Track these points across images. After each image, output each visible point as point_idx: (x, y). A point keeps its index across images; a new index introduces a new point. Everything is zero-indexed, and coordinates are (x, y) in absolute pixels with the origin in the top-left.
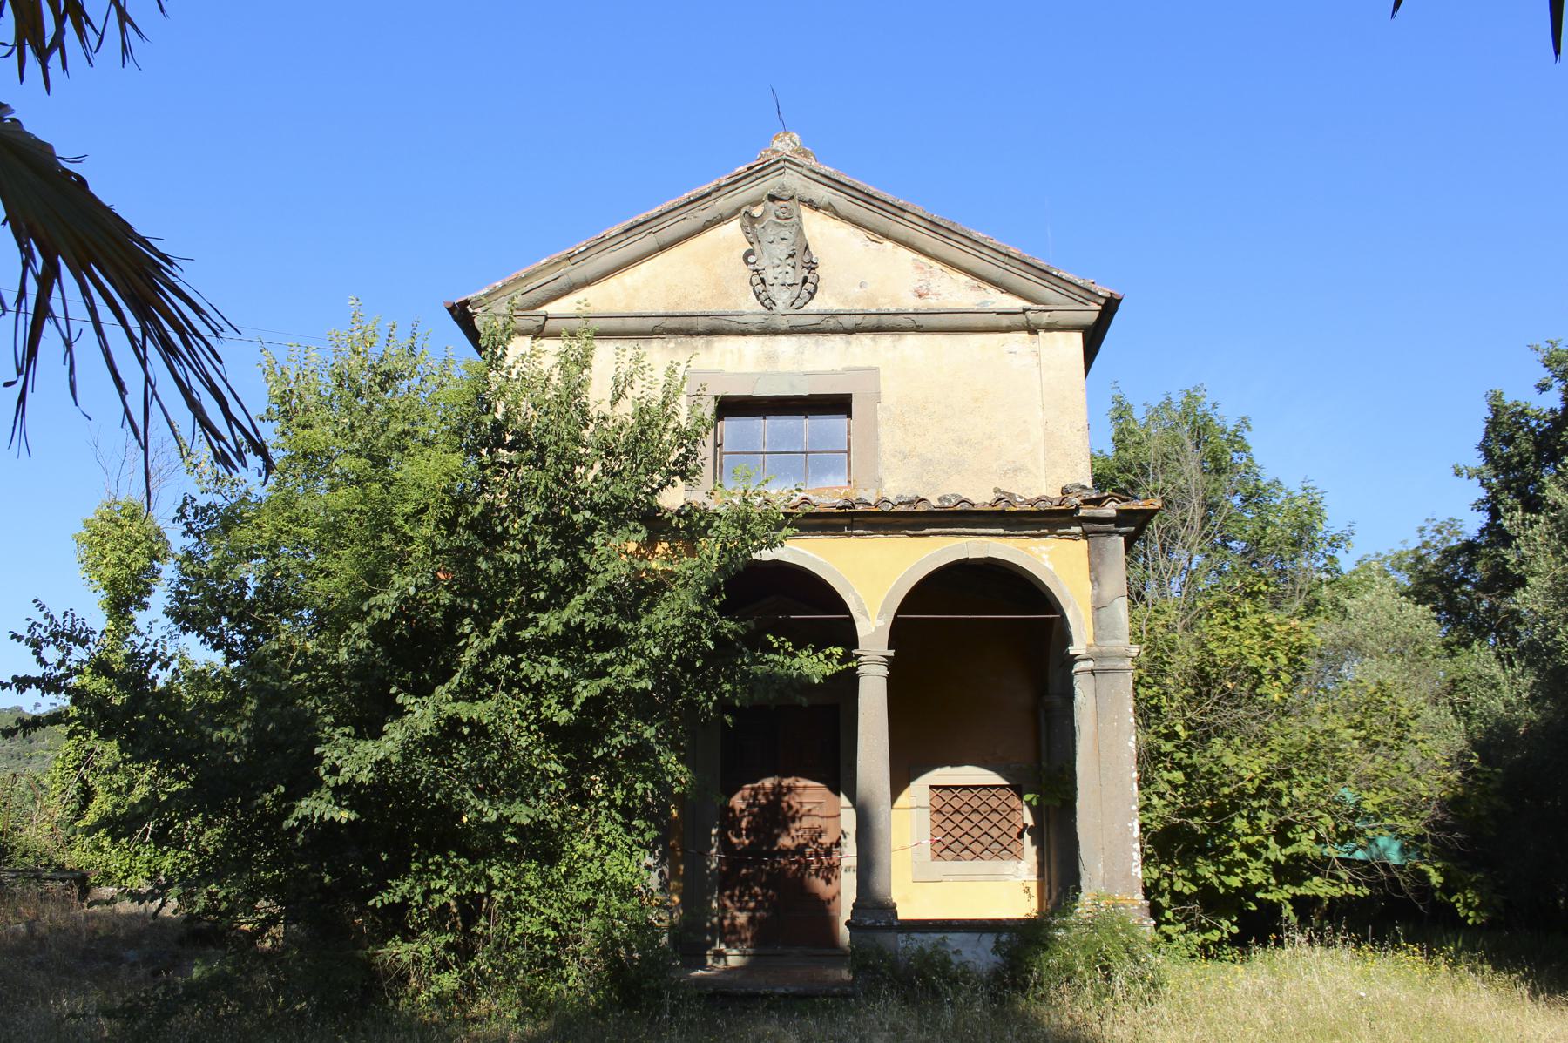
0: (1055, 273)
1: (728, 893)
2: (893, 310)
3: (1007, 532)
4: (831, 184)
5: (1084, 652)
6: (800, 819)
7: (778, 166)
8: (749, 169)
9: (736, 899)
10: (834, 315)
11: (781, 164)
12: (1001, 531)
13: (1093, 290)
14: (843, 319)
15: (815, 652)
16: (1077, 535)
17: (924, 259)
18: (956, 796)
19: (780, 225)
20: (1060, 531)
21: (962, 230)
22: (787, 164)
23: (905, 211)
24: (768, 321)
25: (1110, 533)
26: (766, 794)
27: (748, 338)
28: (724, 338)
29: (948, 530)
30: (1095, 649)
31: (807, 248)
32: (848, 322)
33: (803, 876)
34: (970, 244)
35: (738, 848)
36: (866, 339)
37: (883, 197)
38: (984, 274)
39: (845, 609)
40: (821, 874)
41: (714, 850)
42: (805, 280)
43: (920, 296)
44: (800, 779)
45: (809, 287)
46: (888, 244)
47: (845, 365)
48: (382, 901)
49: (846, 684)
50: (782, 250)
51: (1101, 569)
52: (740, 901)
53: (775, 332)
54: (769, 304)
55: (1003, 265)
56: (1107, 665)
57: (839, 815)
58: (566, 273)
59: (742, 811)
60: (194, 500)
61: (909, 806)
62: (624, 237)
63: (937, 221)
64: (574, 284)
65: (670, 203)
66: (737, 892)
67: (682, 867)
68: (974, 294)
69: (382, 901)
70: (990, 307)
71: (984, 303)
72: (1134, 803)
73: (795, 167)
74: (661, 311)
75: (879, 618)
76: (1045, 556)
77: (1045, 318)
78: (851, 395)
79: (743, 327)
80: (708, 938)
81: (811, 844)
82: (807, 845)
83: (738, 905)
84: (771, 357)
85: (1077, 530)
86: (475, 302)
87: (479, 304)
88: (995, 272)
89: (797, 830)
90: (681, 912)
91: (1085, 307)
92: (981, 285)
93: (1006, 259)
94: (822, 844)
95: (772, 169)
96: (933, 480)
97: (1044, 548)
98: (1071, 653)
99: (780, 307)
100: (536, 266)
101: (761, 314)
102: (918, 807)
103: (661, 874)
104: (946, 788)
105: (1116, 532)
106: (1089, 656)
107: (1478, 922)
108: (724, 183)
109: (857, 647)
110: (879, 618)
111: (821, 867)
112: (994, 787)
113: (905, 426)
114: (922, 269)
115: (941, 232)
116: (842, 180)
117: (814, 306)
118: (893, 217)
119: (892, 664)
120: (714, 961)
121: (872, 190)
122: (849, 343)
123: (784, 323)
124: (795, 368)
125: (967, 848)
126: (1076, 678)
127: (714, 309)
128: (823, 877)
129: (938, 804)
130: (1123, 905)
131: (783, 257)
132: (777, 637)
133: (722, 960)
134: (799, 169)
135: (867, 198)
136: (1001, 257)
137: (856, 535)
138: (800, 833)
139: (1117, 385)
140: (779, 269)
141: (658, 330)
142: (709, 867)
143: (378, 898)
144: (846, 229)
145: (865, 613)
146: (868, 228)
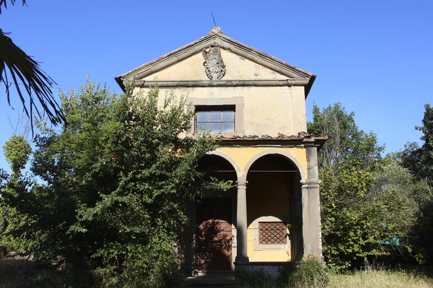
0: (296, 69)
1: (198, 254)
2: (248, 80)
5: (305, 182)
6: (220, 232)
7: (214, 37)
8: (205, 37)
9: (201, 256)
10: (230, 81)
12: (280, 146)
14: (233, 82)
15: (225, 182)
16: (303, 147)
18: (267, 225)
19: (214, 54)
20: (298, 146)
21: (269, 56)
22: (216, 36)
23: (252, 50)
24: (211, 83)
25: (312, 146)
26: (210, 224)
27: (205, 88)
28: (197, 88)
29: (264, 145)
30: (308, 181)
31: (222, 61)
32: (234, 83)
33: (221, 249)
34: (271, 60)
35: (202, 241)
36: (240, 88)
37: (245, 46)
40: (226, 248)
41: (194, 241)
42: (222, 71)
43: (256, 75)
45: (223, 73)
46: (246, 60)
47: (233, 96)
49: (234, 191)
50: (215, 62)
51: (310, 157)
56: (312, 186)
58: (150, 68)
59: (202, 229)
63: (261, 53)
64: (153, 72)
65: (181, 47)
66: (201, 254)
67: (185, 246)
69: (95, 256)
71: (275, 78)
72: (320, 227)
73: (219, 37)
74: (179, 80)
75: (243, 172)
76: (293, 153)
77: (293, 82)
79: (203, 85)
81: (223, 240)
82: (222, 240)
83: (201, 258)
84: (211, 94)
85: (303, 145)
86: (123, 77)
87: (124, 77)
88: (278, 68)
91: (305, 79)
92: (274, 72)
93: (282, 65)
94: (226, 239)
95: (212, 37)
96: (259, 130)
97: (293, 151)
98: (301, 182)
99: (214, 79)
102: (255, 228)
103: (178, 248)
108: (197, 42)
110: (243, 172)
112: (278, 222)
113: (251, 114)
114: (257, 67)
115: (262, 56)
116: (233, 41)
117: (224, 78)
118: (248, 52)
119: (247, 185)
121: (242, 44)
122: (235, 89)
123: (215, 83)
127: (195, 79)
130: (317, 258)
132: (213, 177)
134: (220, 38)
135: (240, 46)
139: (315, 102)
142: (193, 246)
143: (94, 255)
144: (234, 55)
145: (239, 170)
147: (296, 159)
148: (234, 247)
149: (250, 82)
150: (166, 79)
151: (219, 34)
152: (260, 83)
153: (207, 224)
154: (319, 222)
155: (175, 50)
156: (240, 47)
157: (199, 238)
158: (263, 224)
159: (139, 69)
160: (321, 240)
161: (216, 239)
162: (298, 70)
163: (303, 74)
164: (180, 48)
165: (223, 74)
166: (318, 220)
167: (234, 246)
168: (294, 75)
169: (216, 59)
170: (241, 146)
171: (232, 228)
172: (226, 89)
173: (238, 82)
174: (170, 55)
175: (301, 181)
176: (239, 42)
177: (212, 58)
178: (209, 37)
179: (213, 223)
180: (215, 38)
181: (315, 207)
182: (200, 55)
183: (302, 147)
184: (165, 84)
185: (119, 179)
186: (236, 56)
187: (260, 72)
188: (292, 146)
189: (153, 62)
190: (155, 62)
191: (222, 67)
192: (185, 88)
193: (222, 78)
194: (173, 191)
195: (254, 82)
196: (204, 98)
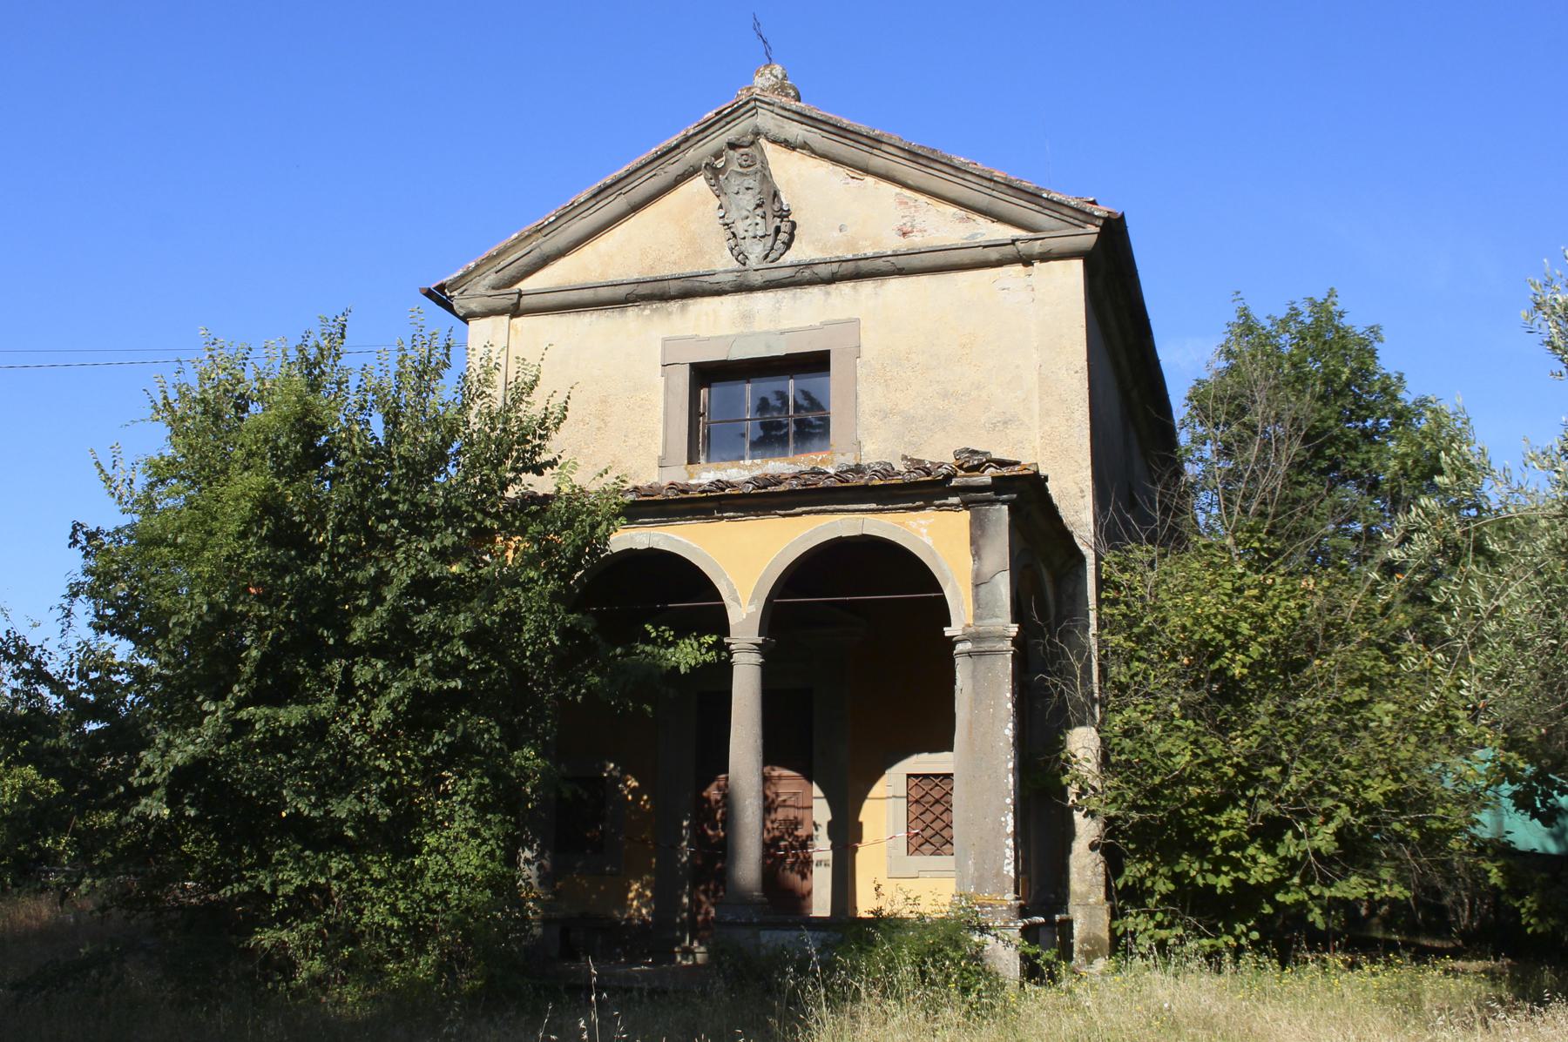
0: (1045, 195)
1: (702, 887)
2: (870, 254)
3: (881, 507)
5: (960, 633)
6: (776, 810)
7: (748, 107)
8: (717, 114)
9: (710, 893)
10: (809, 265)
11: (751, 105)
12: (873, 506)
13: (1087, 210)
16: (958, 506)
18: (937, 785)
20: (937, 502)
21: (943, 157)
22: (758, 103)
23: (881, 142)
24: (741, 279)
25: (991, 502)
28: (699, 300)
29: (819, 508)
30: (972, 630)
32: (823, 271)
33: (777, 870)
34: (952, 171)
35: (713, 841)
36: (845, 288)
37: (857, 129)
38: (970, 203)
39: (718, 596)
40: (796, 868)
41: (685, 843)
42: (778, 230)
43: (904, 234)
44: (776, 768)
45: (783, 237)
46: (870, 180)
47: (823, 319)
48: (232, 890)
49: (720, 672)
50: (748, 200)
51: (981, 542)
52: (715, 895)
53: (751, 289)
54: (741, 256)
55: (989, 191)
56: (985, 646)
57: (811, 807)
58: (538, 246)
59: (717, 802)
60: (82, 526)
61: (885, 796)
62: (593, 202)
63: (916, 150)
64: (548, 257)
65: (638, 160)
66: (712, 887)
67: (654, 860)
68: (962, 226)
69: (232, 890)
70: (981, 240)
71: (973, 236)
72: (1009, 796)
73: (766, 106)
74: (635, 276)
75: (750, 604)
76: (924, 531)
77: (1037, 247)
79: (716, 287)
80: (678, 934)
81: (786, 837)
82: (782, 838)
83: (713, 900)
84: (747, 317)
85: (955, 500)
86: (451, 285)
87: (455, 286)
88: (981, 199)
89: (773, 822)
90: (653, 906)
91: (1081, 231)
92: (970, 215)
93: (991, 185)
94: (797, 837)
95: (742, 110)
96: (915, 439)
97: (923, 522)
98: (947, 634)
99: (753, 262)
101: (733, 271)
102: (894, 797)
103: (540, 868)
104: (926, 776)
105: (998, 501)
106: (965, 637)
107: (1540, 930)
108: (691, 132)
109: (728, 635)
110: (750, 604)
111: (796, 861)
113: (886, 381)
114: (907, 203)
115: (921, 161)
116: (814, 115)
117: (790, 257)
118: (870, 150)
119: (762, 648)
120: (683, 958)
121: (845, 122)
122: (828, 293)
123: (757, 278)
124: (770, 327)
125: (927, 841)
126: (958, 660)
127: (688, 270)
128: (798, 872)
129: (916, 794)
130: (991, 905)
131: (751, 208)
133: (691, 957)
134: (771, 108)
135: (842, 132)
136: (986, 183)
137: (727, 518)
138: (776, 825)
140: (748, 221)
142: (680, 860)
143: (229, 887)
144: (826, 166)
145: (736, 600)
146: (847, 165)
147: (932, 553)
149: (880, 261)
150: (594, 277)
151: (766, 94)
152: (916, 261)
154: (1007, 777)
155: (615, 171)
156: (842, 133)
157: (704, 831)
158: (913, 781)
159: (500, 254)
160: (1010, 842)
162: (1051, 201)
163: (1071, 213)
165: (783, 243)
167: (819, 859)
168: (1040, 219)
169: (750, 191)
170: (740, 514)
171: (814, 795)
172: (798, 295)
173: (835, 267)
174: (601, 191)
175: (948, 632)
177: (736, 189)
178: (729, 109)
180: (754, 111)
182: (699, 183)
184: (587, 295)
185: (243, 655)
186: (831, 167)
187: (920, 220)
188: (917, 503)
189: (546, 223)
190: (550, 223)
191: (779, 217)
192: (659, 305)
193: (782, 255)
194: (453, 684)
196: (721, 337)
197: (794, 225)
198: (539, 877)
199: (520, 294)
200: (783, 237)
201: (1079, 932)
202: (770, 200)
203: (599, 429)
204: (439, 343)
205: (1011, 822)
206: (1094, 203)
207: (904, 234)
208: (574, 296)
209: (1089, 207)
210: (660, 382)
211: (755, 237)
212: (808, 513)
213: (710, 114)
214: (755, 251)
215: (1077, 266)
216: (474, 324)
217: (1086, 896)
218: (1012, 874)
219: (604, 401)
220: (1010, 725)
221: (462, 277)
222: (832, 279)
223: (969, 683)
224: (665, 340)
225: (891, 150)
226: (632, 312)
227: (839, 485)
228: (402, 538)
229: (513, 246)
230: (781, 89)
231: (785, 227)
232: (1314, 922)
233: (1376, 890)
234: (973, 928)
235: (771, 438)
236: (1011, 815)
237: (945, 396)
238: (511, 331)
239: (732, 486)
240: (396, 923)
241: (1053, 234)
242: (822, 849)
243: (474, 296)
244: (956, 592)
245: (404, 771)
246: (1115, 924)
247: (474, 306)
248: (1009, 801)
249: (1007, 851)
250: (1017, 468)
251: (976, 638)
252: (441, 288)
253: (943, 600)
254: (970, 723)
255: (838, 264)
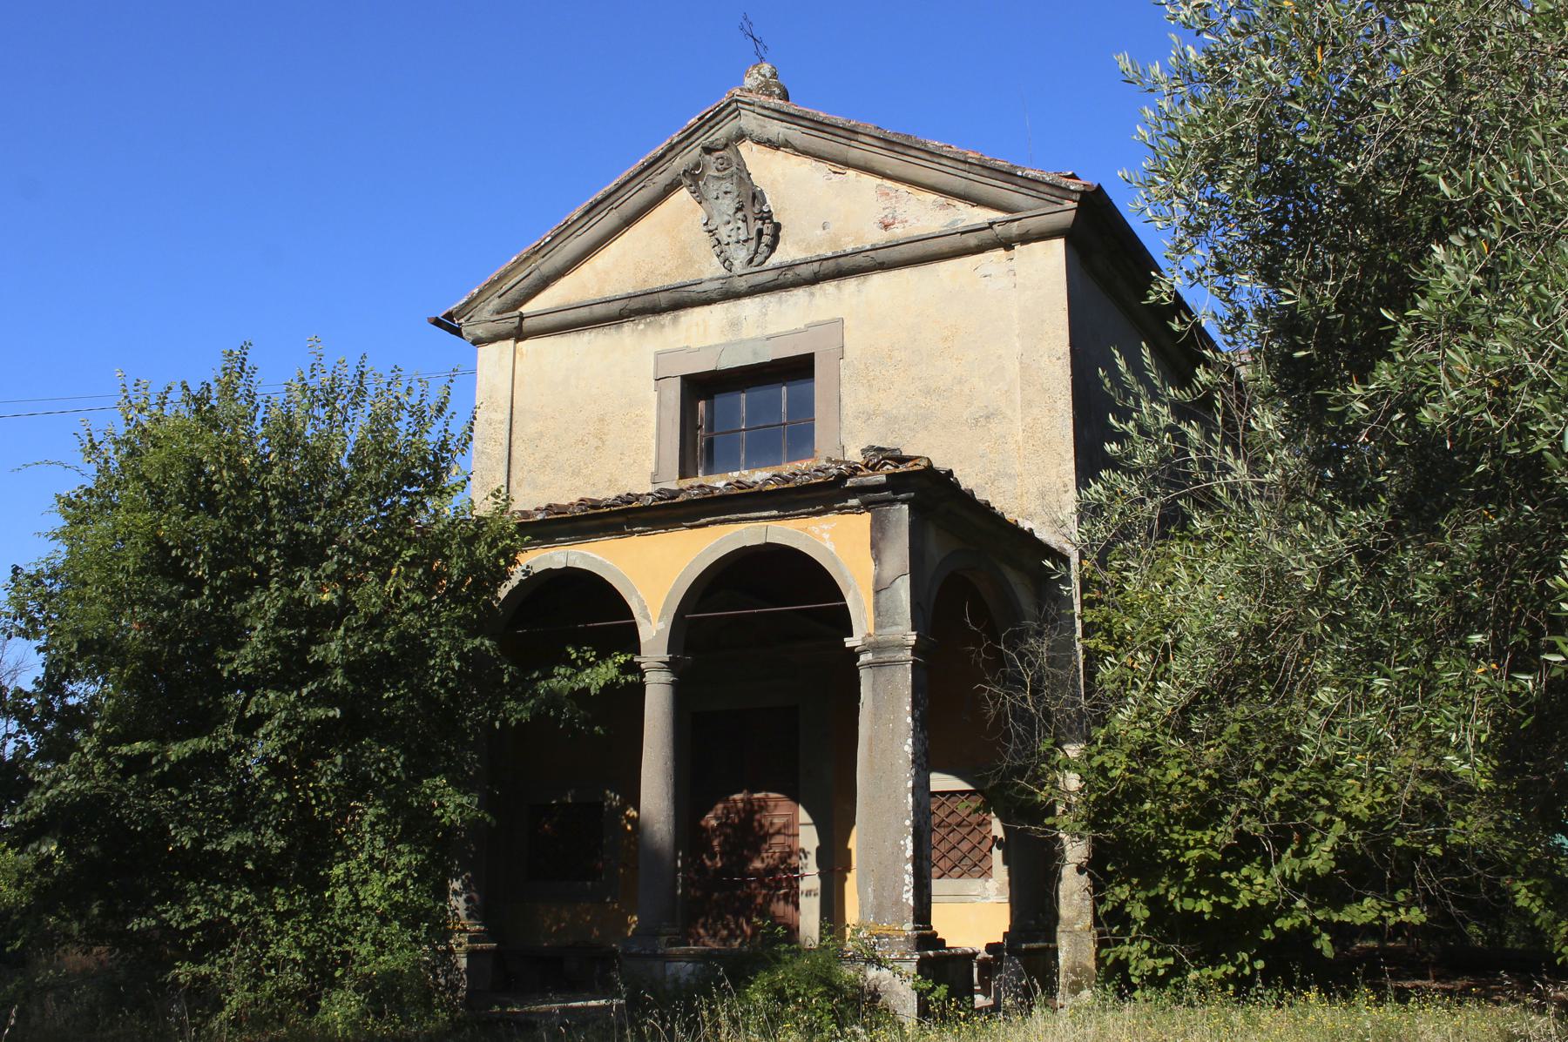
0: (1019, 173)
2: (849, 250)
4: (782, 117)
5: (860, 643)
7: (730, 109)
8: (700, 119)
10: (791, 266)
11: (732, 108)
12: (775, 513)
16: (858, 508)
17: (888, 183)
20: (837, 506)
21: (917, 142)
23: (857, 133)
24: (727, 286)
25: (892, 502)
26: (738, 812)
28: (690, 311)
30: (871, 639)
32: (805, 271)
36: (829, 287)
38: (948, 189)
42: (760, 233)
43: (886, 227)
45: (766, 239)
46: (851, 173)
47: (807, 321)
50: (728, 205)
51: (881, 545)
54: (726, 262)
55: (965, 174)
56: (885, 656)
58: (538, 268)
62: (586, 219)
65: (626, 173)
70: (960, 226)
71: (954, 223)
74: (620, 293)
76: (826, 536)
77: (1015, 228)
78: (812, 355)
79: (704, 296)
85: (854, 502)
87: (461, 314)
88: (958, 183)
91: (1059, 208)
92: (950, 201)
93: (967, 167)
95: (724, 113)
97: (825, 527)
99: (738, 267)
100: (507, 265)
101: (718, 279)
109: (639, 653)
112: (953, 793)
115: (897, 149)
116: (792, 111)
117: (776, 259)
119: (671, 665)
121: (822, 115)
123: (742, 284)
126: (862, 673)
127: (678, 281)
130: (888, 936)
131: (731, 213)
134: (752, 108)
135: (819, 126)
136: (961, 166)
141: (625, 313)
144: (807, 164)
145: (647, 617)
148: (808, 893)
150: (592, 294)
152: (895, 254)
153: (727, 811)
156: (819, 127)
159: (500, 279)
160: (909, 867)
161: (758, 864)
162: (1026, 178)
163: (1047, 190)
164: (623, 176)
166: (902, 789)
168: (1017, 199)
175: (849, 642)
176: (811, 111)
179: (748, 802)
181: (892, 739)
182: (683, 196)
183: (855, 510)
186: (814, 163)
191: (760, 219)
193: (767, 258)
194: (331, 714)
195: (871, 254)
197: (778, 227)
198: (467, 909)
199: (522, 317)
200: (766, 239)
201: (1065, 961)
202: (752, 200)
203: (596, 448)
204: (351, 371)
205: (910, 846)
206: (1073, 176)
207: (886, 227)
208: (571, 316)
209: (1064, 182)
210: (653, 396)
211: (738, 242)
212: (714, 523)
213: (693, 120)
214: (740, 255)
215: (1059, 245)
216: (483, 351)
217: (1072, 923)
218: (911, 902)
219: (602, 420)
220: (910, 741)
221: (467, 303)
222: (815, 280)
223: (870, 695)
224: (658, 354)
225: (868, 140)
226: (627, 327)
227: (739, 491)
228: (277, 567)
229: (512, 270)
230: (765, 88)
231: (768, 229)
232: (1322, 949)
233: (1391, 914)
234: (869, 961)
235: (763, 449)
236: (910, 838)
237: (928, 392)
238: (518, 355)
239: (638, 497)
240: (299, 956)
241: (1030, 213)
242: (811, 881)
243: (479, 322)
244: (858, 600)
245: (314, 802)
246: (1104, 952)
247: (480, 331)
248: (908, 823)
249: (907, 877)
250: (910, 464)
251: (876, 648)
252: (449, 316)
253: (845, 607)
254: (871, 738)
255: (818, 264)
